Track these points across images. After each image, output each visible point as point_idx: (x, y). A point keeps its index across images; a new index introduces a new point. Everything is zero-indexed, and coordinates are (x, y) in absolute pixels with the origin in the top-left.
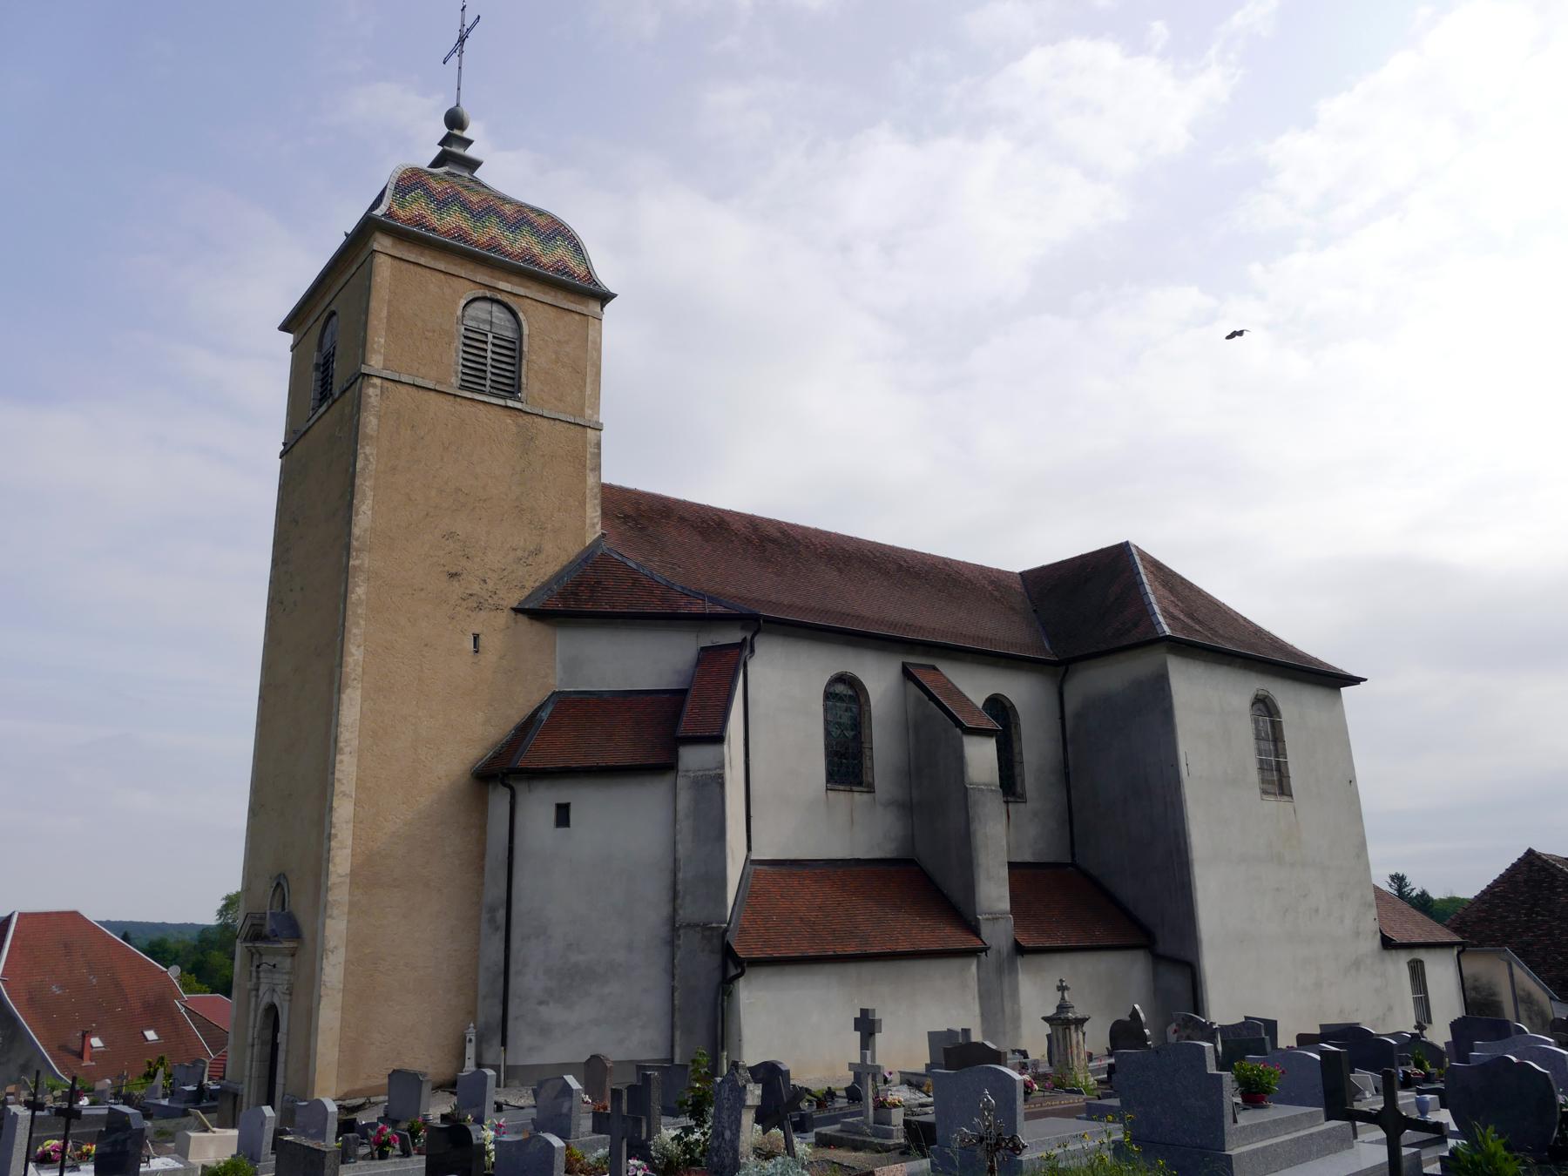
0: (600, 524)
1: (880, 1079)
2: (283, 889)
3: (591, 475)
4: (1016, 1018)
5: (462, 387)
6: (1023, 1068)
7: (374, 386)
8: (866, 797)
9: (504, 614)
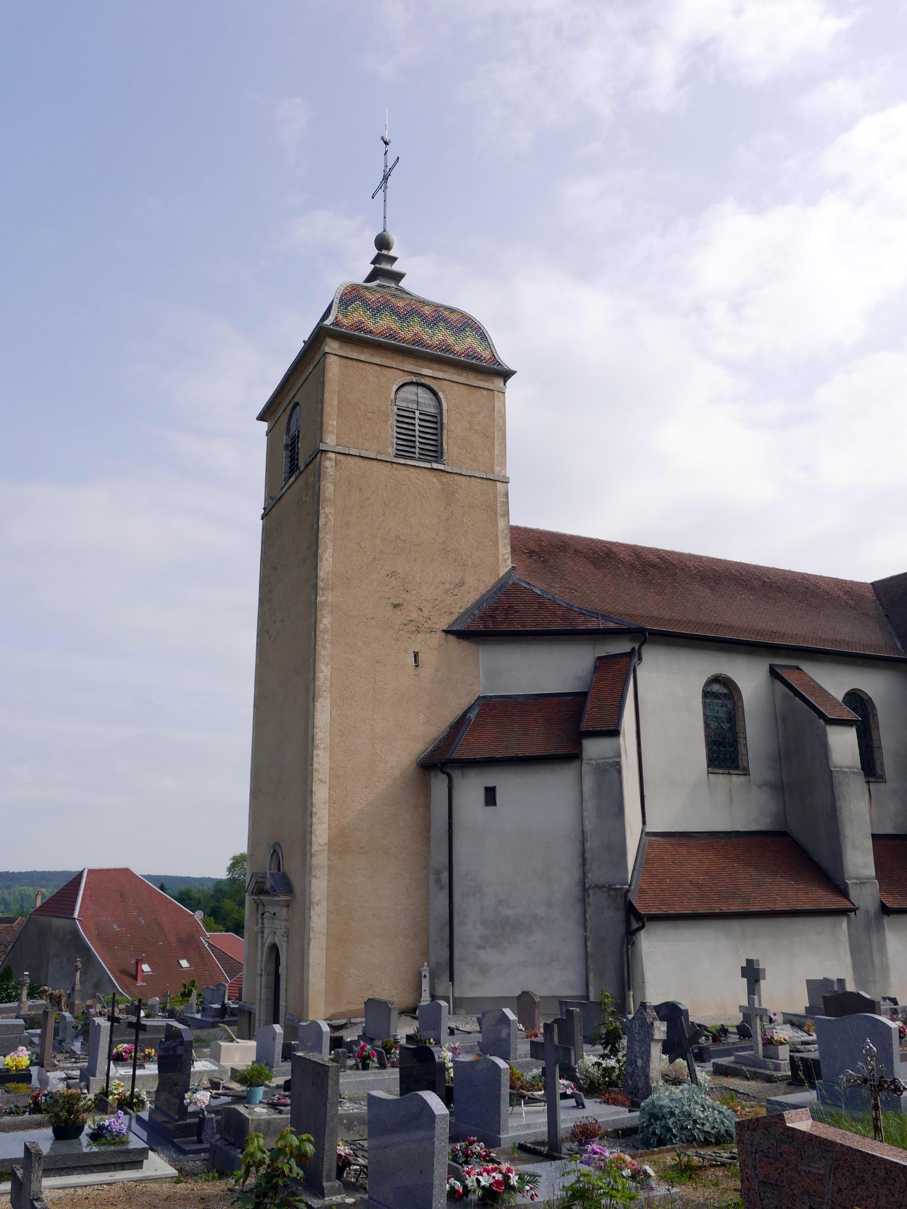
0: (510, 559)
1: (766, 1019)
2: (278, 854)
3: (502, 520)
4: (885, 969)
5: (397, 456)
6: (894, 1014)
7: (330, 459)
8: (742, 779)
9: (437, 635)
